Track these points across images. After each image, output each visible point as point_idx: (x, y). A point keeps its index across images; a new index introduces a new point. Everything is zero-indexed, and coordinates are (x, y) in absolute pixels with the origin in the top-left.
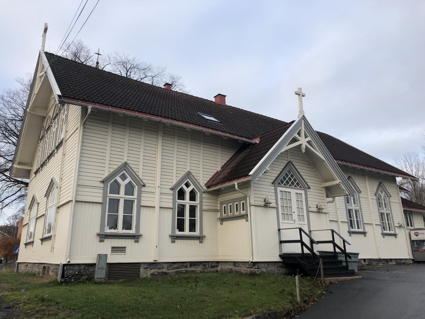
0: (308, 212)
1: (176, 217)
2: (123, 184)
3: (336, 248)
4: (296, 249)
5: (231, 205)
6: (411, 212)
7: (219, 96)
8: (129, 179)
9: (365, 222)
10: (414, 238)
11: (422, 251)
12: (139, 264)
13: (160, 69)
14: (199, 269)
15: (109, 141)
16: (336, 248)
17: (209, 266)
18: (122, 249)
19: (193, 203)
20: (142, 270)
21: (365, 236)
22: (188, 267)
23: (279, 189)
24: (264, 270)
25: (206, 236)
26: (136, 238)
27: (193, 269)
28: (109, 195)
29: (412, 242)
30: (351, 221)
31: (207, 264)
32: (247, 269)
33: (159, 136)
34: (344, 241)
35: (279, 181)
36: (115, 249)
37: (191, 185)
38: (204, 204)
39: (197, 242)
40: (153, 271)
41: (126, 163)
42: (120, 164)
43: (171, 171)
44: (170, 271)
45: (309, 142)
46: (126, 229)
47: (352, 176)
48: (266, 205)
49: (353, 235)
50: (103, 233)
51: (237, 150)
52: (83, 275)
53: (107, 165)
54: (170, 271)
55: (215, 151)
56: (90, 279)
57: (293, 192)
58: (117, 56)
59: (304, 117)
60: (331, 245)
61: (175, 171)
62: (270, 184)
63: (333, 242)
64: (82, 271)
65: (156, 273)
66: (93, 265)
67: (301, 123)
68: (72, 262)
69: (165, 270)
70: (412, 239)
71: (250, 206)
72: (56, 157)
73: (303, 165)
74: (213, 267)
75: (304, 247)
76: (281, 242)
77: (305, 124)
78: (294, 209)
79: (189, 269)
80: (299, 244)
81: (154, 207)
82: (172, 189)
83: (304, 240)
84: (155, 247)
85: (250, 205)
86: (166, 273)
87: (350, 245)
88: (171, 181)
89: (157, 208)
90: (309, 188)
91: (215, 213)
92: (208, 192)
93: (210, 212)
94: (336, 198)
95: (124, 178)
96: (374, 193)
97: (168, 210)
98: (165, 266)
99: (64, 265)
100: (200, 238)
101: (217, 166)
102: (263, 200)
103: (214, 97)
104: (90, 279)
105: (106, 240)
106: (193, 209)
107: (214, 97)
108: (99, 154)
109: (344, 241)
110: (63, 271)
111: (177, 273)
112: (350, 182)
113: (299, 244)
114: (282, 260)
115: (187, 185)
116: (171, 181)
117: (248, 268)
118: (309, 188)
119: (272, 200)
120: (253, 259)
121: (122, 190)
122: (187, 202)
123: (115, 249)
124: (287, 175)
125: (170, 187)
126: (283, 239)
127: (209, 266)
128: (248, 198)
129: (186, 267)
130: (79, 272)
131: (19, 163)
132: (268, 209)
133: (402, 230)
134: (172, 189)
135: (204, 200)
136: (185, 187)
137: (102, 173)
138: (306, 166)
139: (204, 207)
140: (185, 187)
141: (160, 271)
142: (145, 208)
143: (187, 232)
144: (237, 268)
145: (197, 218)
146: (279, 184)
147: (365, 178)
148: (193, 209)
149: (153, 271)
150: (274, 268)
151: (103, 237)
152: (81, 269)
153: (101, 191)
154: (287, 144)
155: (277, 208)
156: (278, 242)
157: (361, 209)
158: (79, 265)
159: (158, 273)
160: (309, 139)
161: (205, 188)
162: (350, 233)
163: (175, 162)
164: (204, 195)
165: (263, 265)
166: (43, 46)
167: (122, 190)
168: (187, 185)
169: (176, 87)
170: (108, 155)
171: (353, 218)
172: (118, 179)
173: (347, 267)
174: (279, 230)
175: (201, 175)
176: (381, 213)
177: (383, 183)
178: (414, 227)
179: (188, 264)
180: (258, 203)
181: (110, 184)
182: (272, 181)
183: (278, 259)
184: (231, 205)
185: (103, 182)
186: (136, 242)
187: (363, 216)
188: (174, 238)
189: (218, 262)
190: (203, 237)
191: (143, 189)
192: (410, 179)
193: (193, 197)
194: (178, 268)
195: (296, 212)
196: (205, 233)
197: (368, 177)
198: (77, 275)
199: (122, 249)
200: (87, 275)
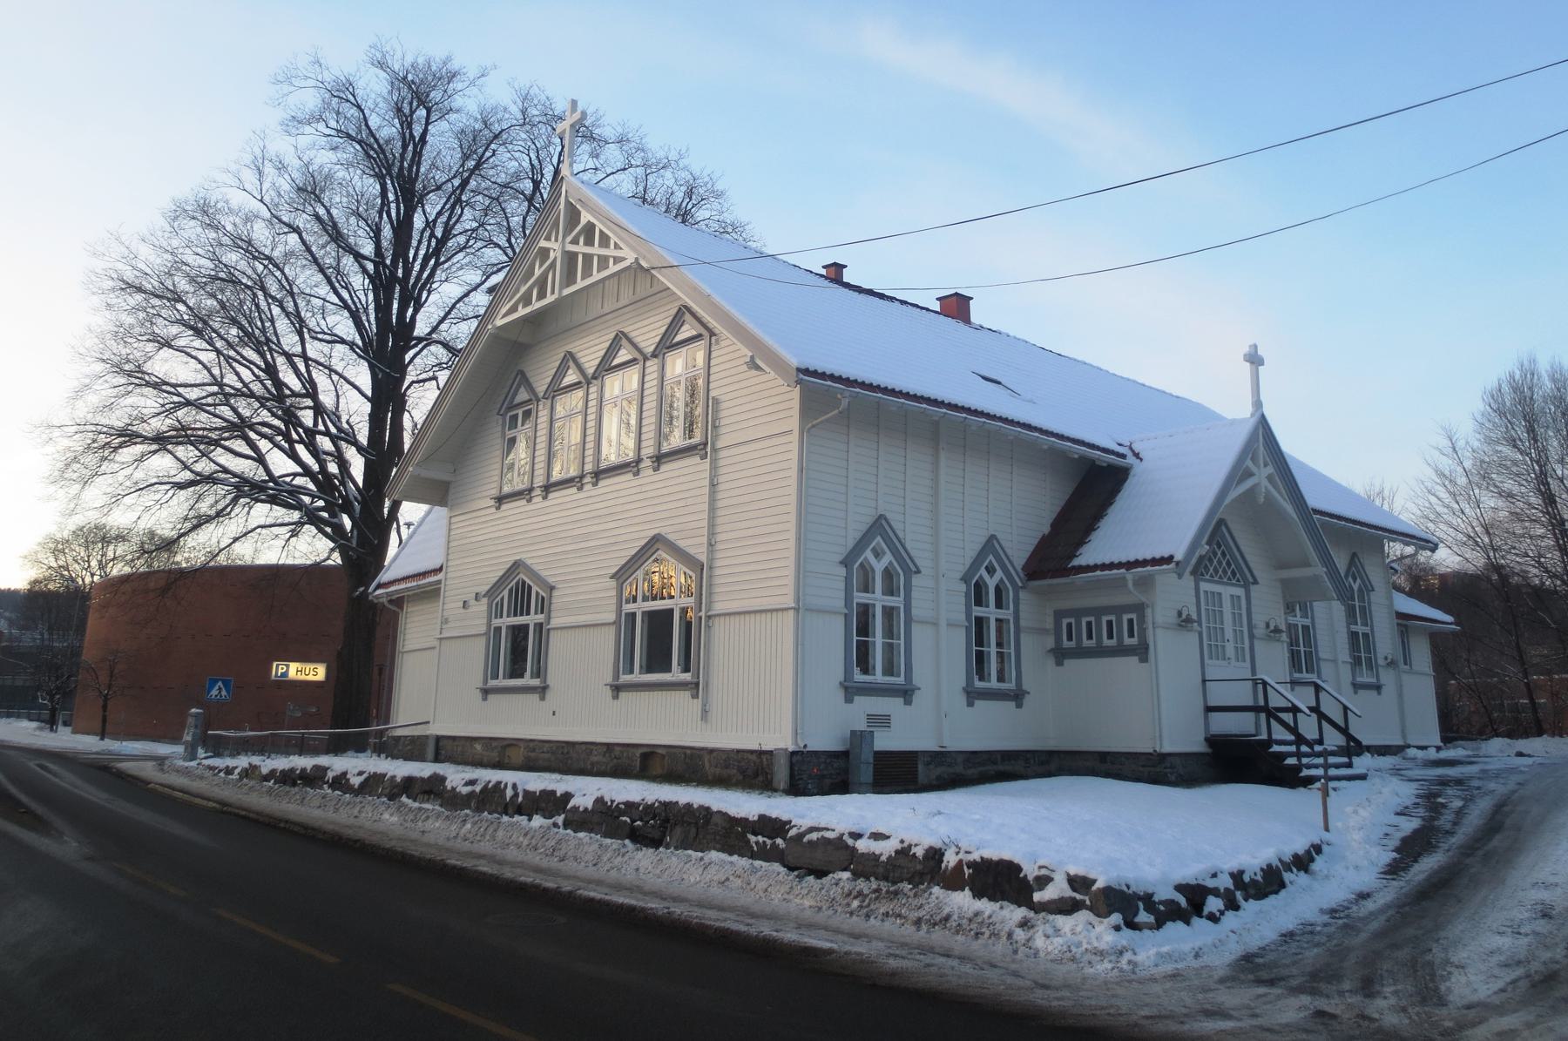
0: (1252, 637)
1: (855, 638)
7: (954, 298)
12: (916, 752)
19: (1002, 614)
20: (921, 767)
21: (1379, 693)
23: (1204, 586)
25: (919, 689)
26: (906, 693)
28: (855, 594)
32: (1141, 769)
34: (1346, 708)
39: (536, 697)
49: (1361, 692)
57: (1228, 591)
59: (1263, 423)
71: (1154, 628)
72: (641, 481)
76: (1210, 709)
78: (1229, 634)
83: (1323, 709)
89: (943, 623)
90: (1256, 582)
94: (369, 404)
96: (723, 406)
99: (793, 753)
100: (1017, 697)
103: (937, 299)
107: (937, 299)
110: (792, 766)
112: (412, 281)
115: (991, 570)
117: (1143, 766)
118: (1256, 582)
126: (1212, 703)
139: (1023, 623)
162: (1357, 687)
168: (991, 570)
173: (1297, 769)
174: (1204, 681)
177: (1360, 555)
188: (972, 695)
195: (1231, 639)
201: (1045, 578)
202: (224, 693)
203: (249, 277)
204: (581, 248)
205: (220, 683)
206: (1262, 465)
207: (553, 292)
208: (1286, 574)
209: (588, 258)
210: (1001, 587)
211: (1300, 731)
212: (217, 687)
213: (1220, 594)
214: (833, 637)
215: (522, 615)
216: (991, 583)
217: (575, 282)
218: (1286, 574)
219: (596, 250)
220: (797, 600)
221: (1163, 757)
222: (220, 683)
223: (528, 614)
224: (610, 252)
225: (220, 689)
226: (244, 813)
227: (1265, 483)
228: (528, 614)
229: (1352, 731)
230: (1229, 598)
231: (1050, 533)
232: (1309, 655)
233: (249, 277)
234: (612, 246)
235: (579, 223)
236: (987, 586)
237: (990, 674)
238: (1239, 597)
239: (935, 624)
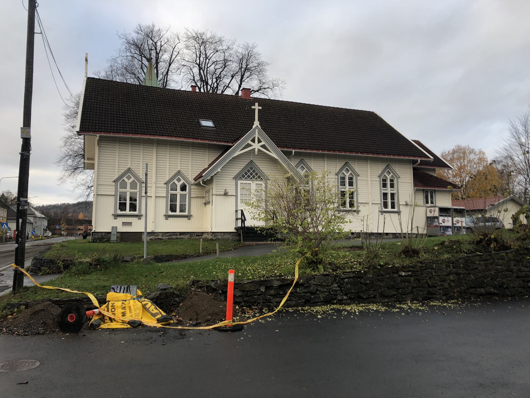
2: (129, 182)
5: (351, 173)
6: (435, 191)
8: (133, 179)
10: (429, 215)
11: (433, 227)
13: (230, 42)
14: (187, 237)
15: (117, 154)
17: (195, 235)
18: (130, 224)
22: (178, 235)
23: (239, 182)
24: (220, 237)
27: (182, 237)
28: (119, 190)
29: (428, 218)
31: (194, 233)
33: (154, 147)
36: (124, 224)
38: (192, 193)
40: (151, 237)
41: (129, 168)
42: (126, 169)
43: (165, 171)
44: (164, 238)
46: (133, 211)
47: (348, 162)
48: (226, 194)
50: (116, 214)
51: (224, 150)
52: (105, 239)
53: (117, 170)
54: (164, 238)
55: (204, 151)
56: (108, 241)
58: (188, 32)
61: (168, 171)
64: (103, 236)
65: (154, 239)
66: (110, 233)
67: (255, 131)
68: (97, 231)
69: (160, 237)
70: (428, 216)
71: (212, 195)
73: (267, 162)
74: (199, 236)
77: (259, 132)
79: (179, 237)
81: (152, 197)
84: (152, 222)
86: (160, 239)
88: (165, 178)
91: (202, 199)
92: (196, 184)
93: (198, 199)
95: (129, 178)
97: (163, 198)
98: (160, 234)
100: (189, 217)
101: (205, 164)
102: (224, 191)
104: (108, 241)
105: (118, 218)
111: (169, 239)
114: (236, 231)
116: (165, 178)
119: (232, 192)
121: (128, 186)
123: (124, 224)
124: (249, 171)
125: (164, 182)
127: (195, 235)
128: (211, 190)
129: (177, 236)
130: (102, 237)
131: (88, 159)
132: (228, 196)
133: (408, 208)
135: (192, 191)
136: (176, 182)
137: (114, 175)
138: (271, 162)
139: (192, 196)
141: (157, 237)
142: (149, 197)
143: (178, 213)
144: (145, 236)
146: (241, 178)
147: (367, 162)
149: (151, 237)
150: (229, 236)
151: (116, 216)
152: (103, 235)
153: (114, 188)
154: (240, 150)
155: (236, 196)
156: (235, 219)
157: (357, 191)
158: (101, 232)
159: (155, 238)
161: (193, 182)
163: (168, 164)
164: (192, 187)
165: (219, 234)
166: (86, 73)
167: (128, 186)
169: (252, 57)
170: (117, 164)
172: (125, 178)
175: (190, 172)
177: (390, 164)
178: (436, 204)
179: (178, 234)
180: (218, 193)
181: (120, 183)
183: (234, 231)
184: (351, 173)
185: (114, 182)
186: (139, 219)
187: (380, 195)
188: (167, 217)
189: (203, 233)
190: (190, 216)
194: (169, 236)
196: (192, 213)
197: (370, 160)
198: (101, 238)
199: (130, 224)
200: (107, 238)
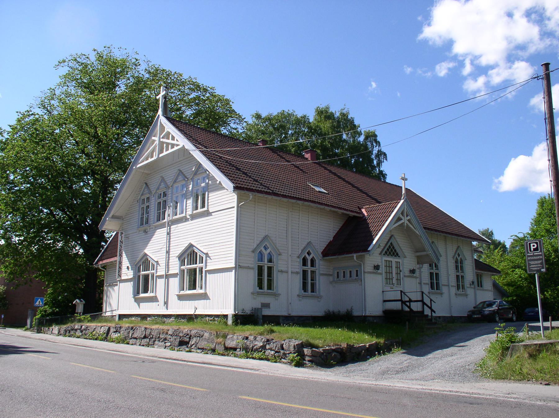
3: (409, 305)
4: (397, 306)
9: (366, 270)
16: (409, 305)
26: (276, 295)
30: (431, 283)
34: (431, 300)
35: (384, 252)
37: (269, 248)
38: (321, 269)
45: (409, 220)
60: (420, 304)
62: (378, 255)
63: (422, 301)
75: (430, 306)
76: (385, 301)
80: (400, 302)
82: (298, 257)
83: (425, 301)
85: (364, 272)
87: (435, 303)
89: (290, 273)
106: (313, 272)
108: (226, 229)
109: (431, 300)
113: (400, 302)
120: (195, 312)
122: (309, 268)
134: (298, 257)
136: (307, 256)
140: (307, 256)
145: (316, 281)
146: (384, 254)
148: (313, 272)
160: (409, 218)
171: (434, 280)
174: (383, 292)
176: (457, 275)
182: (379, 252)
191: (279, 257)
192: (307, 159)
193: (313, 265)
201: (343, 254)
202: (41, 303)
203: (135, 237)
204: (165, 140)
205: (39, 300)
206: (406, 216)
207: (156, 156)
208: (418, 254)
209: (168, 144)
210: (313, 259)
211: (430, 310)
212: (38, 301)
213: (392, 261)
214: (252, 276)
215: (147, 271)
216: (309, 258)
217: (163, 152)
218: (418, 254)
219: (170, 141)
220: (236, 264)
221: (366, 317)
222: (39, 300)
223: (196, 264)
224: (175, 142)
225: (39, 302)
226: (167, 269)
227: (406, 222)
228: (196, 264)
229: (433, 308)
230: (394, 262)
231: (333, 240)
232: (438, 284)
233: (135, 237)
234: (175, 140)
235: (164, 131)
236: (308, 259)
237: (308, 290)
238: (399, 262)
239: (287, 272)
